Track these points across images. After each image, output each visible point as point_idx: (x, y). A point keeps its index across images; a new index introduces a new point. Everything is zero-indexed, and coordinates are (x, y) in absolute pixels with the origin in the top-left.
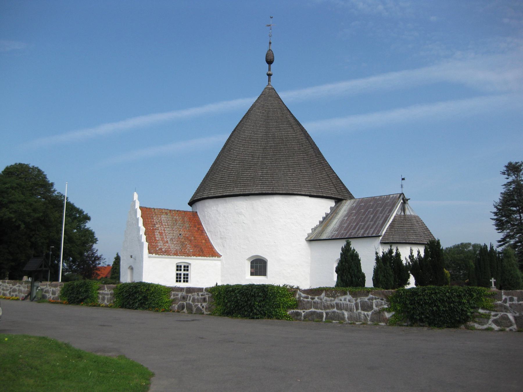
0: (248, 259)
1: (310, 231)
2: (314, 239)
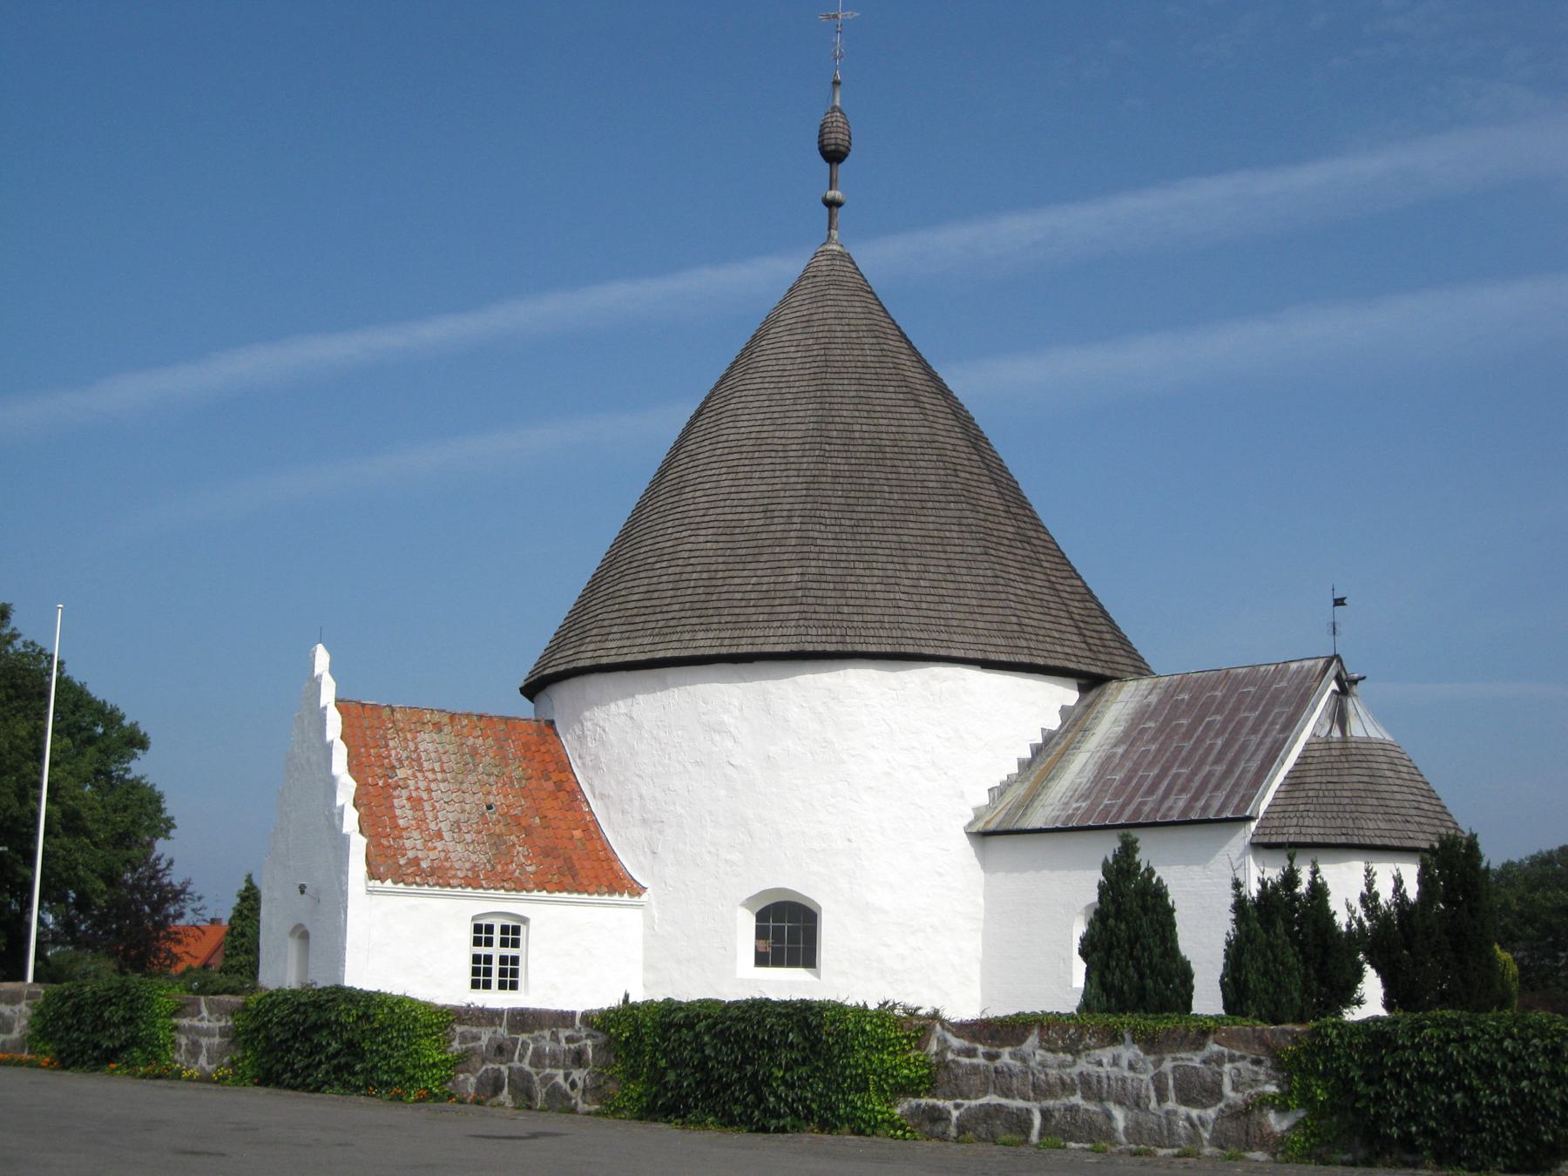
1: (984, 799)
2: (1000, 829)
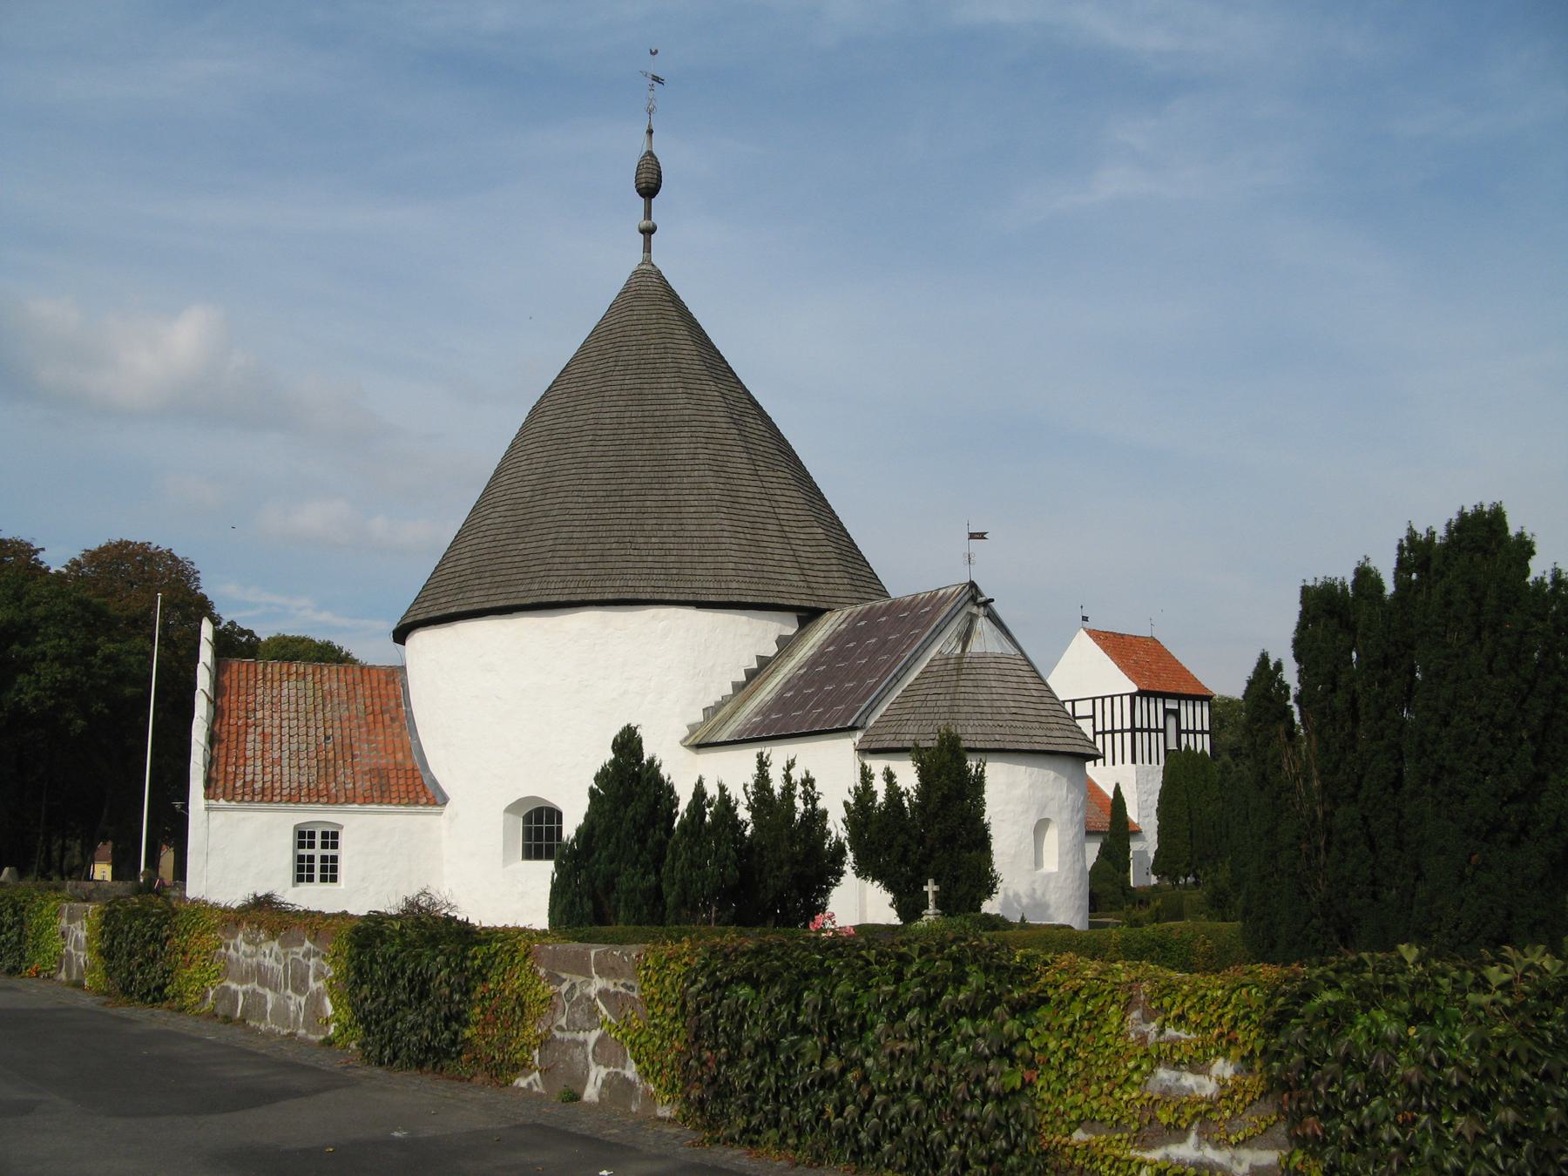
0: (511, 809)
1: (699, 717)
2: (703, 742)
